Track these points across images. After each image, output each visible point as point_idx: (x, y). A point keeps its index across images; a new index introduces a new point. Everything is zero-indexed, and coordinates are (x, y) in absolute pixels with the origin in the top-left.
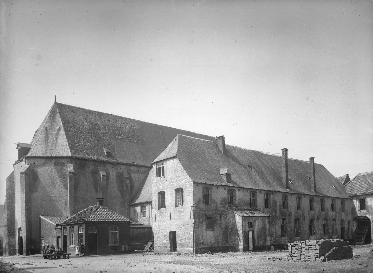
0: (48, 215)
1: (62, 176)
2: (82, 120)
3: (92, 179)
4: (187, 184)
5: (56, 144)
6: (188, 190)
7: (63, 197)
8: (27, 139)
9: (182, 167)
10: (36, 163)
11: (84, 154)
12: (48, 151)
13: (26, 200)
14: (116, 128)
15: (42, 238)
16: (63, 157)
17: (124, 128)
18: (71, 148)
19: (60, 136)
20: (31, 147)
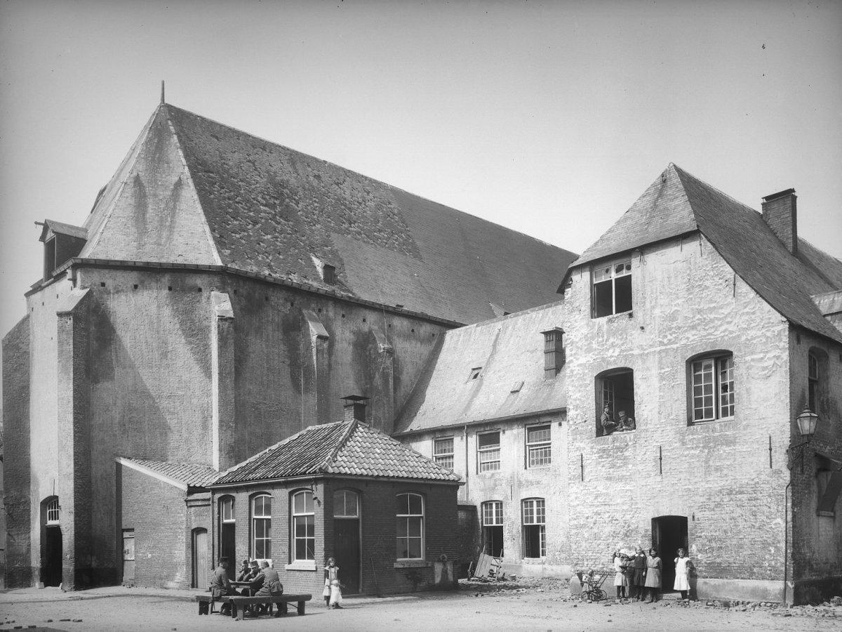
0: (144, 459)
1: (195, 332)
2: (245, 166)
3: (282, 347)
4: (752, 333)
5: (171, 228)
6: (762, 355)
7: (195, 401)
8: (74, 215)
9: (728, 269)
10: (110, 283)
11: (258, 264)
12: (148, 248)
13: (75, 406)
14: (340, 200)
15: (126, 535)
16: (197, 270)
17: (360, 203)
18: (220, 243)
19: (183, 206)
20: (88, 238)
